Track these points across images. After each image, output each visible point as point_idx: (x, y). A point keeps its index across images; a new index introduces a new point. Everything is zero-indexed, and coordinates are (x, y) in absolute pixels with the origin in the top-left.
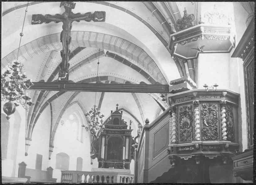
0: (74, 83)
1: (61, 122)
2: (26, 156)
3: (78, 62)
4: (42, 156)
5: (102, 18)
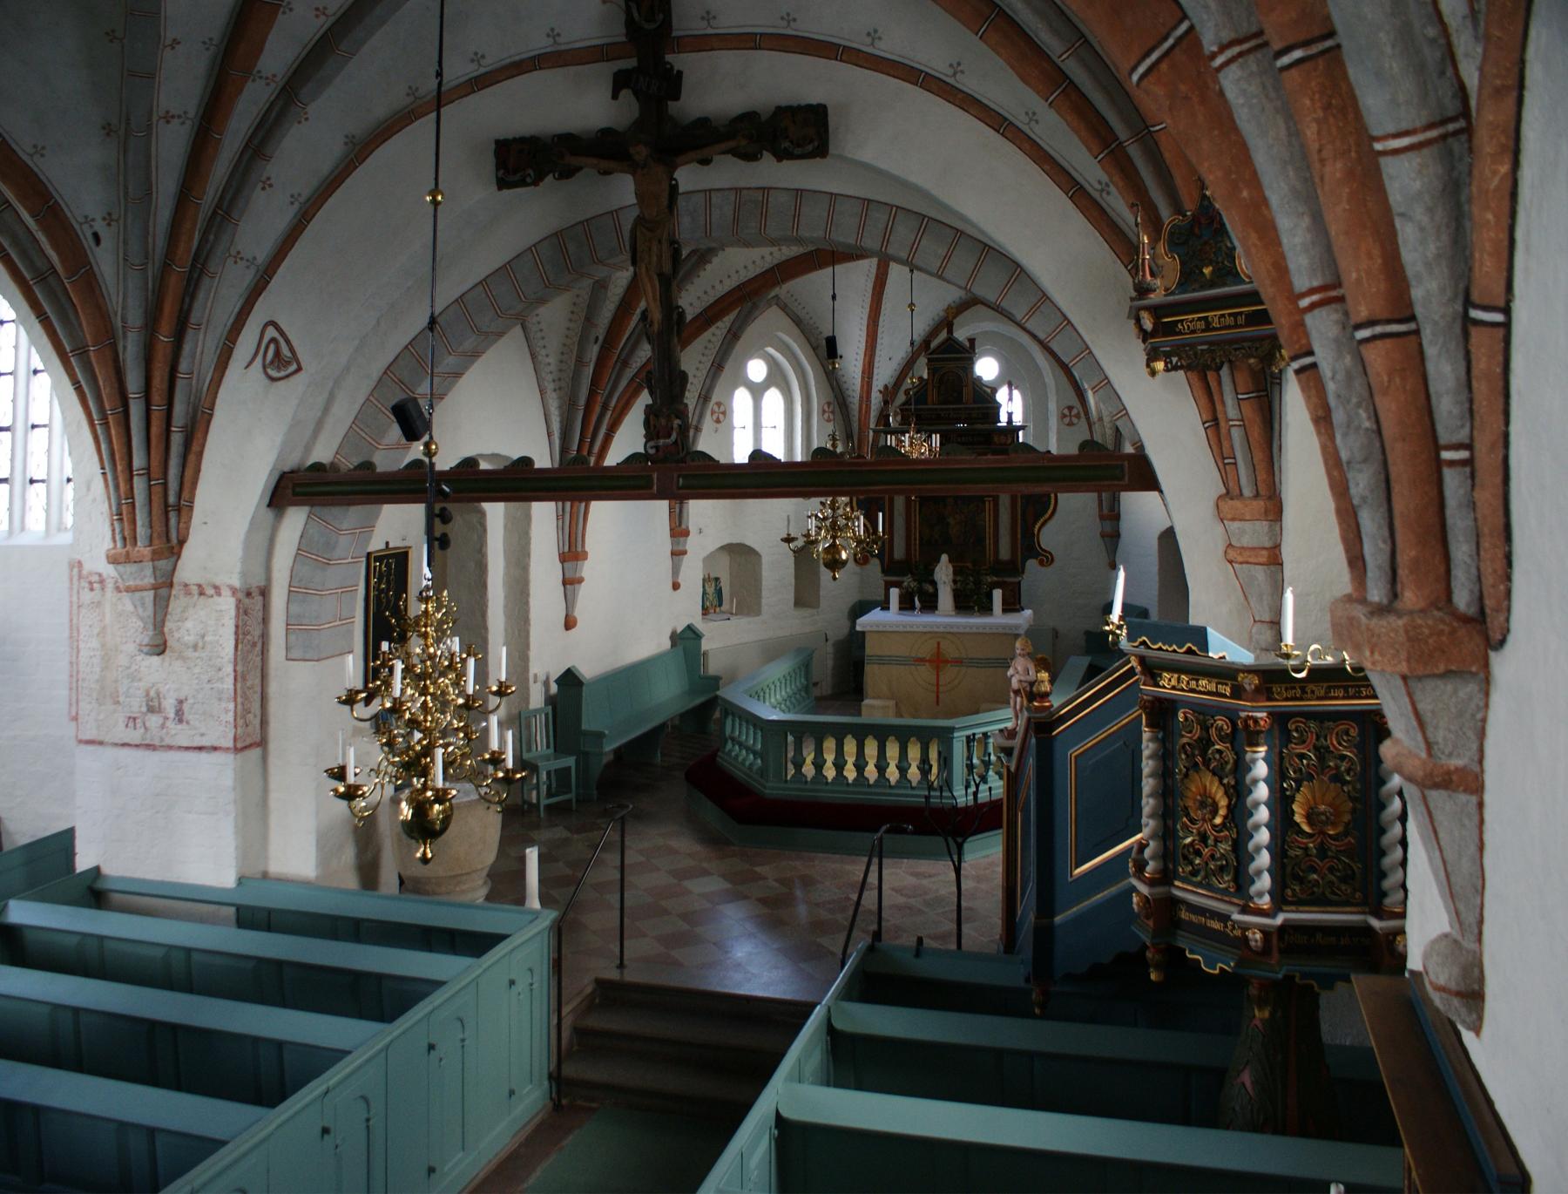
1: (713, 412)
2: (569, 632)
5: (811, 141)
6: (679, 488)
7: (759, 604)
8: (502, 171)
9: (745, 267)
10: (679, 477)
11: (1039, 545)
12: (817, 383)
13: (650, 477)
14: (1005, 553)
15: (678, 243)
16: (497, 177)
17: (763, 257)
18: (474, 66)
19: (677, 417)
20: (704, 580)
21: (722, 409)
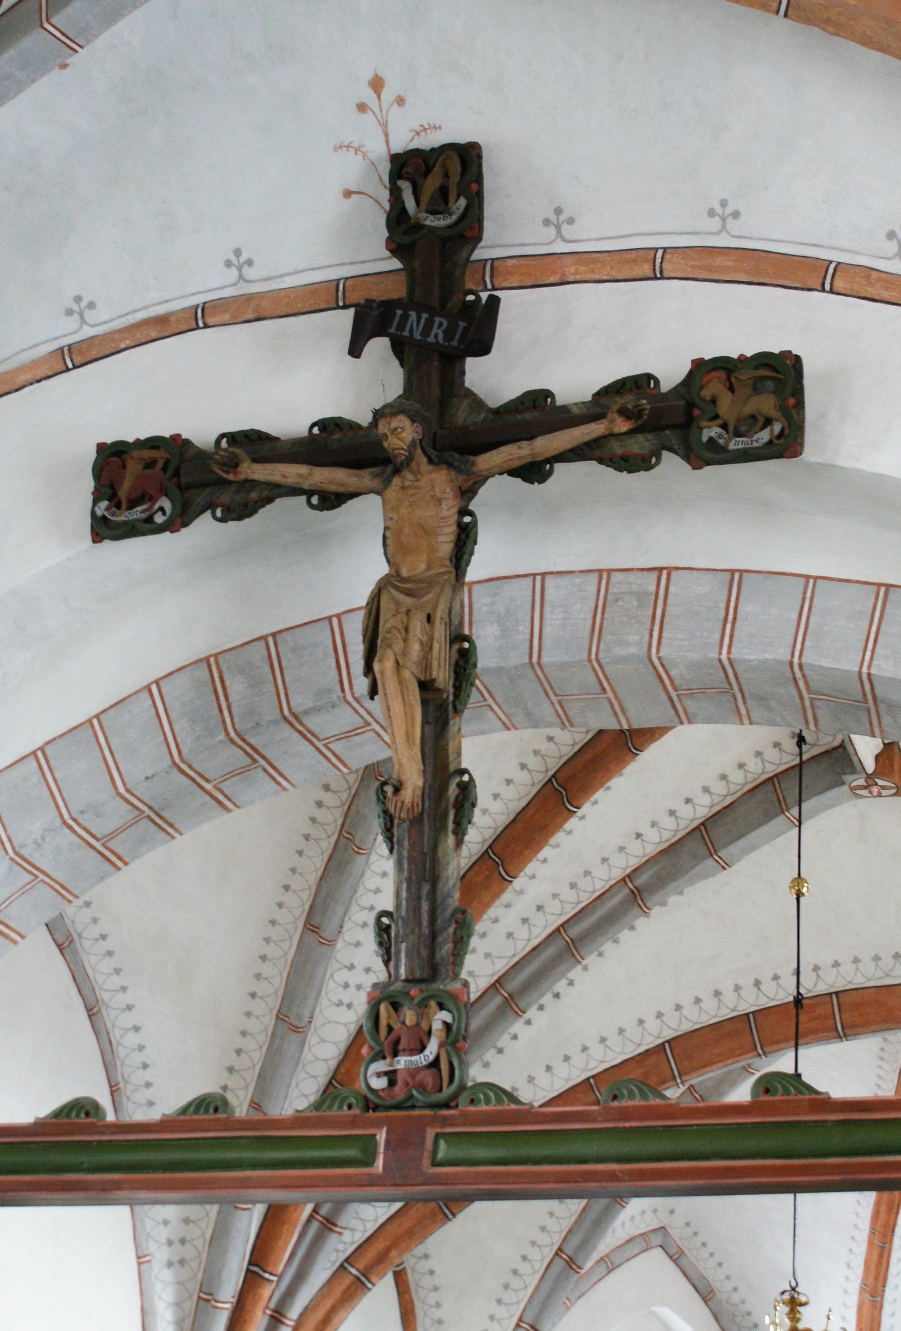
0: (527, 1114)
3: (618, 874)
5: (768, 422)
6: (435, 1163)
8: (104, 504)
9: (603, 1040)
10: (438, 1136)
13: (370, 1142)
15: (468, 639)
16: (93, 513)
17: (641, 1022)
18: (72, 323)
19: (442, 1007)
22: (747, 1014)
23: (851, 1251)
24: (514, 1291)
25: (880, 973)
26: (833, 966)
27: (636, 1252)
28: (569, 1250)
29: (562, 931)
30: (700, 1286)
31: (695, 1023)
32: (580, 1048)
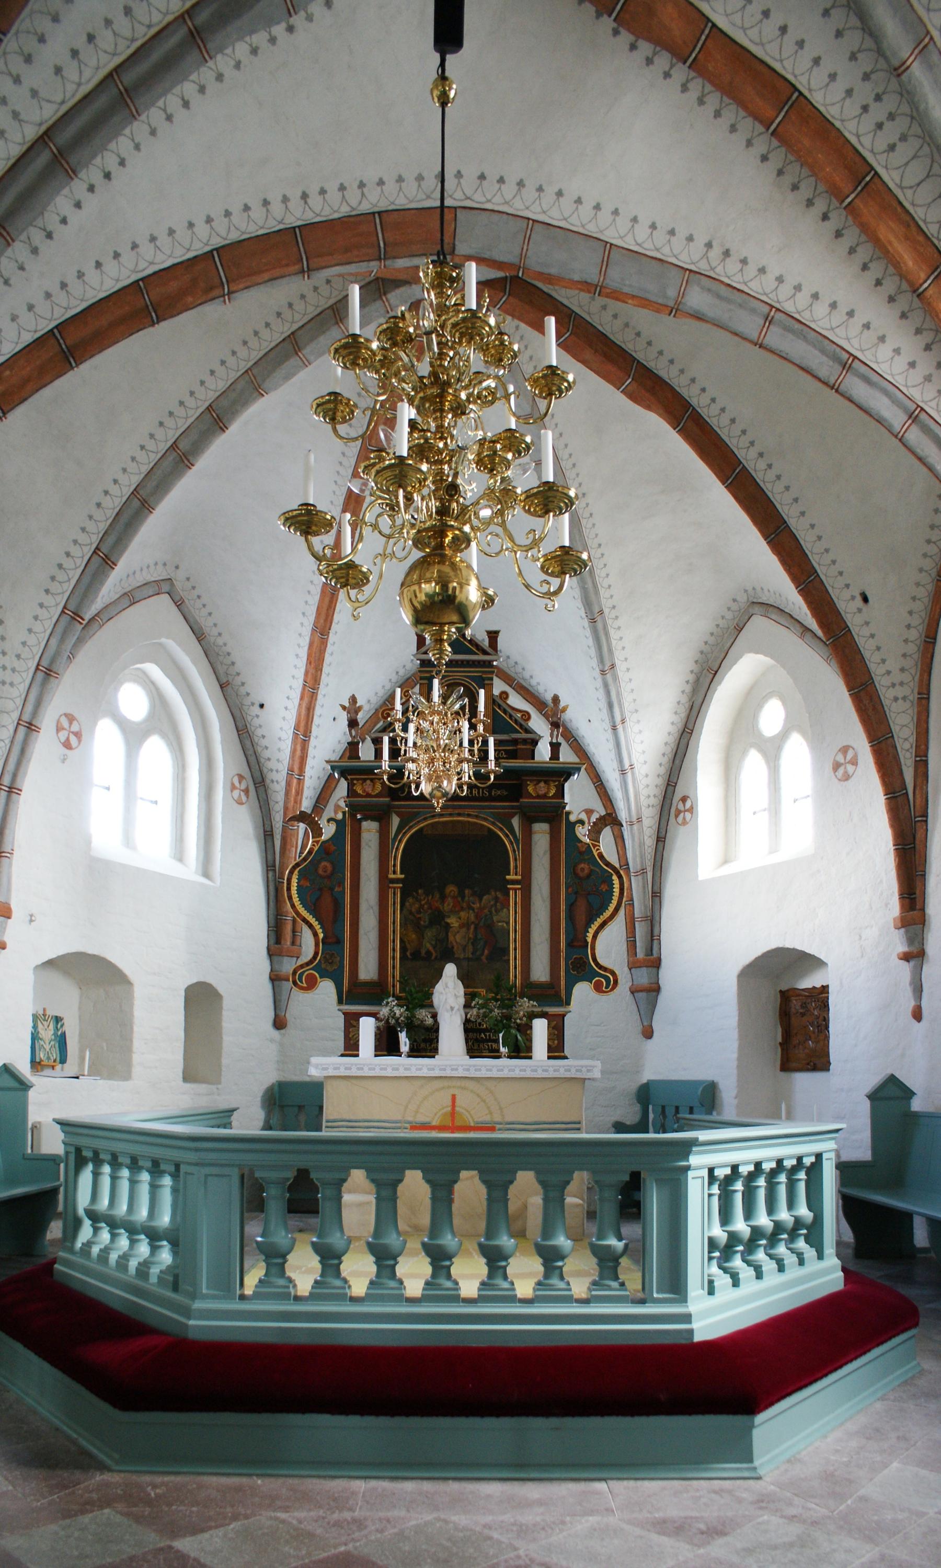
1: (59, 729)
4: (892, 1075)
7: (128, 1065)
11: (595, 960)
12: (223, 741)
14: (540, 972)
17: (191, 225)
20: (35, 1017)
21: (75, 727)
22: (294, 228)
23: (306, 602)
24: (60, 582)
25: (421, 196)
26: (378, 184)
27: (151, 593)
28: (105, 548)
29: (116, 77)
30: (195, 627)
31: (243, 233)
32: (130, 246)
